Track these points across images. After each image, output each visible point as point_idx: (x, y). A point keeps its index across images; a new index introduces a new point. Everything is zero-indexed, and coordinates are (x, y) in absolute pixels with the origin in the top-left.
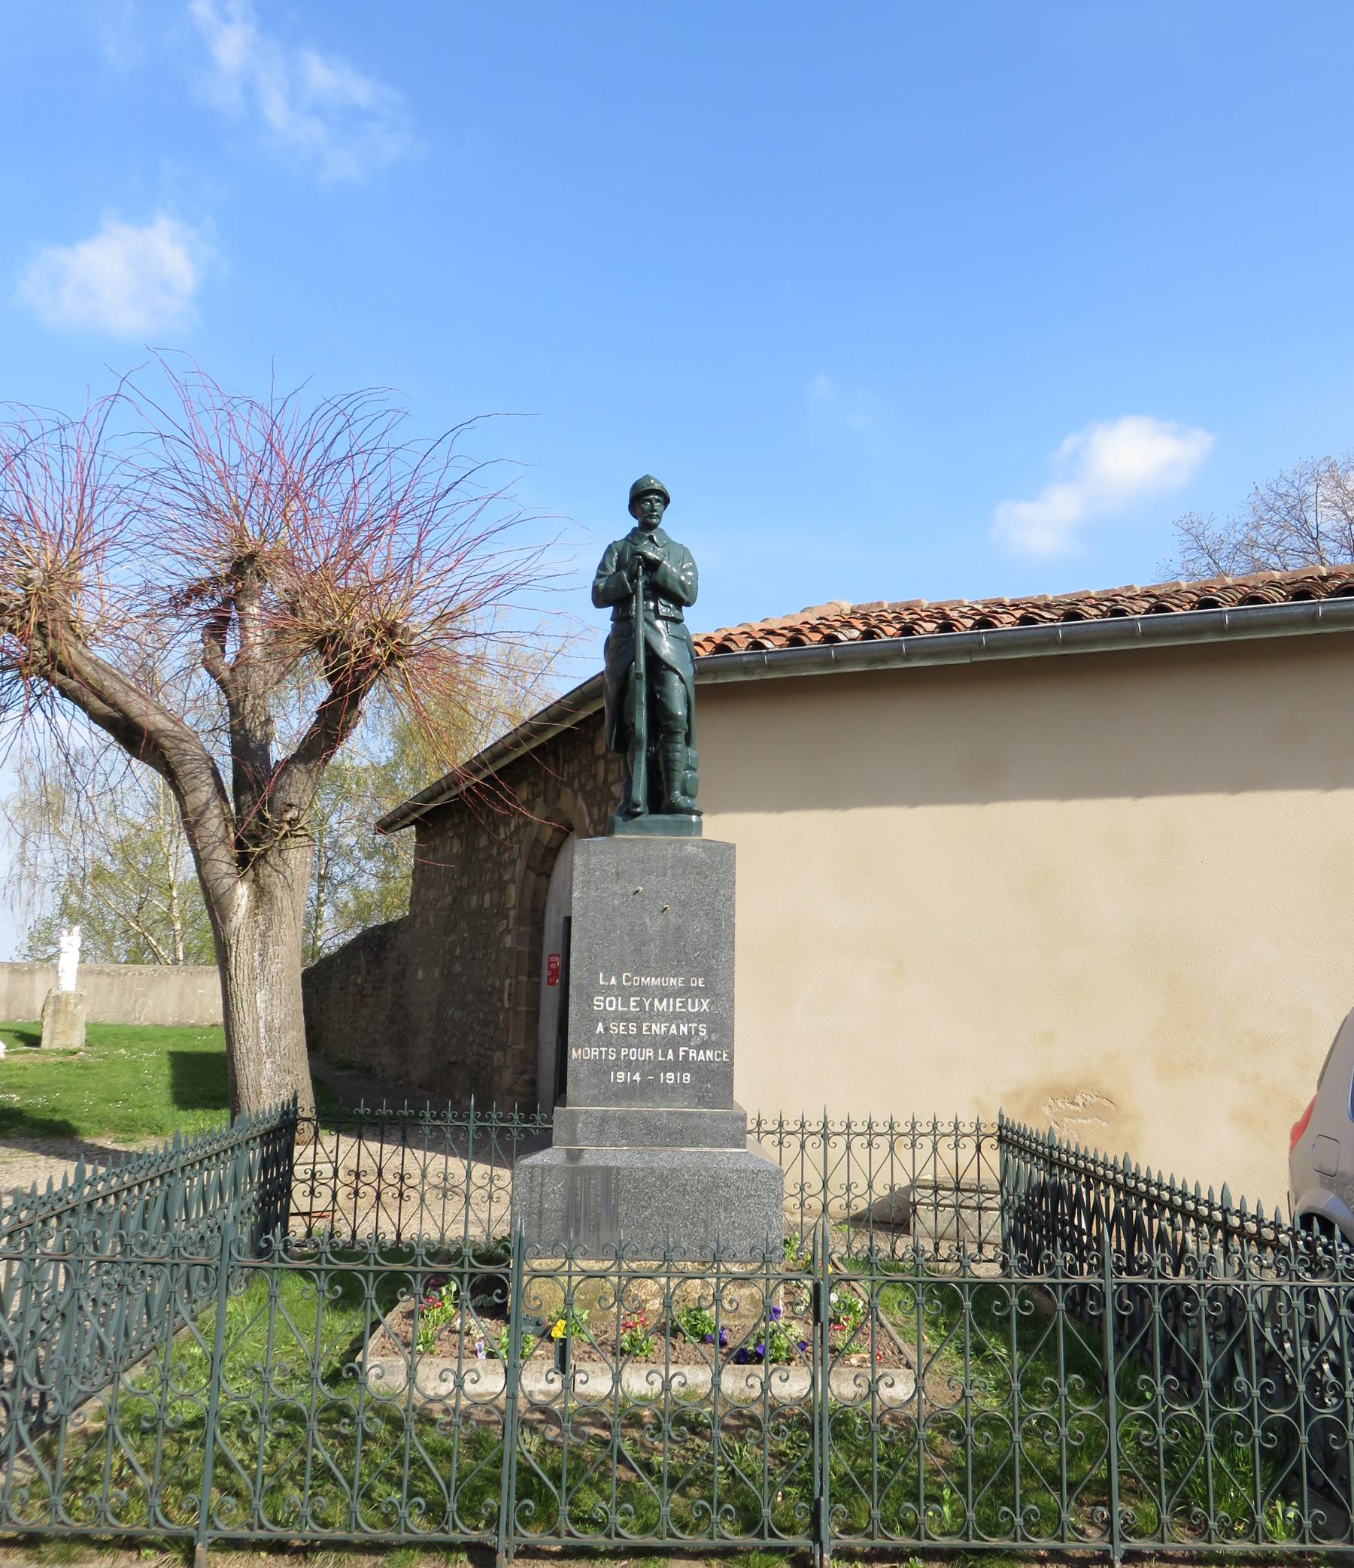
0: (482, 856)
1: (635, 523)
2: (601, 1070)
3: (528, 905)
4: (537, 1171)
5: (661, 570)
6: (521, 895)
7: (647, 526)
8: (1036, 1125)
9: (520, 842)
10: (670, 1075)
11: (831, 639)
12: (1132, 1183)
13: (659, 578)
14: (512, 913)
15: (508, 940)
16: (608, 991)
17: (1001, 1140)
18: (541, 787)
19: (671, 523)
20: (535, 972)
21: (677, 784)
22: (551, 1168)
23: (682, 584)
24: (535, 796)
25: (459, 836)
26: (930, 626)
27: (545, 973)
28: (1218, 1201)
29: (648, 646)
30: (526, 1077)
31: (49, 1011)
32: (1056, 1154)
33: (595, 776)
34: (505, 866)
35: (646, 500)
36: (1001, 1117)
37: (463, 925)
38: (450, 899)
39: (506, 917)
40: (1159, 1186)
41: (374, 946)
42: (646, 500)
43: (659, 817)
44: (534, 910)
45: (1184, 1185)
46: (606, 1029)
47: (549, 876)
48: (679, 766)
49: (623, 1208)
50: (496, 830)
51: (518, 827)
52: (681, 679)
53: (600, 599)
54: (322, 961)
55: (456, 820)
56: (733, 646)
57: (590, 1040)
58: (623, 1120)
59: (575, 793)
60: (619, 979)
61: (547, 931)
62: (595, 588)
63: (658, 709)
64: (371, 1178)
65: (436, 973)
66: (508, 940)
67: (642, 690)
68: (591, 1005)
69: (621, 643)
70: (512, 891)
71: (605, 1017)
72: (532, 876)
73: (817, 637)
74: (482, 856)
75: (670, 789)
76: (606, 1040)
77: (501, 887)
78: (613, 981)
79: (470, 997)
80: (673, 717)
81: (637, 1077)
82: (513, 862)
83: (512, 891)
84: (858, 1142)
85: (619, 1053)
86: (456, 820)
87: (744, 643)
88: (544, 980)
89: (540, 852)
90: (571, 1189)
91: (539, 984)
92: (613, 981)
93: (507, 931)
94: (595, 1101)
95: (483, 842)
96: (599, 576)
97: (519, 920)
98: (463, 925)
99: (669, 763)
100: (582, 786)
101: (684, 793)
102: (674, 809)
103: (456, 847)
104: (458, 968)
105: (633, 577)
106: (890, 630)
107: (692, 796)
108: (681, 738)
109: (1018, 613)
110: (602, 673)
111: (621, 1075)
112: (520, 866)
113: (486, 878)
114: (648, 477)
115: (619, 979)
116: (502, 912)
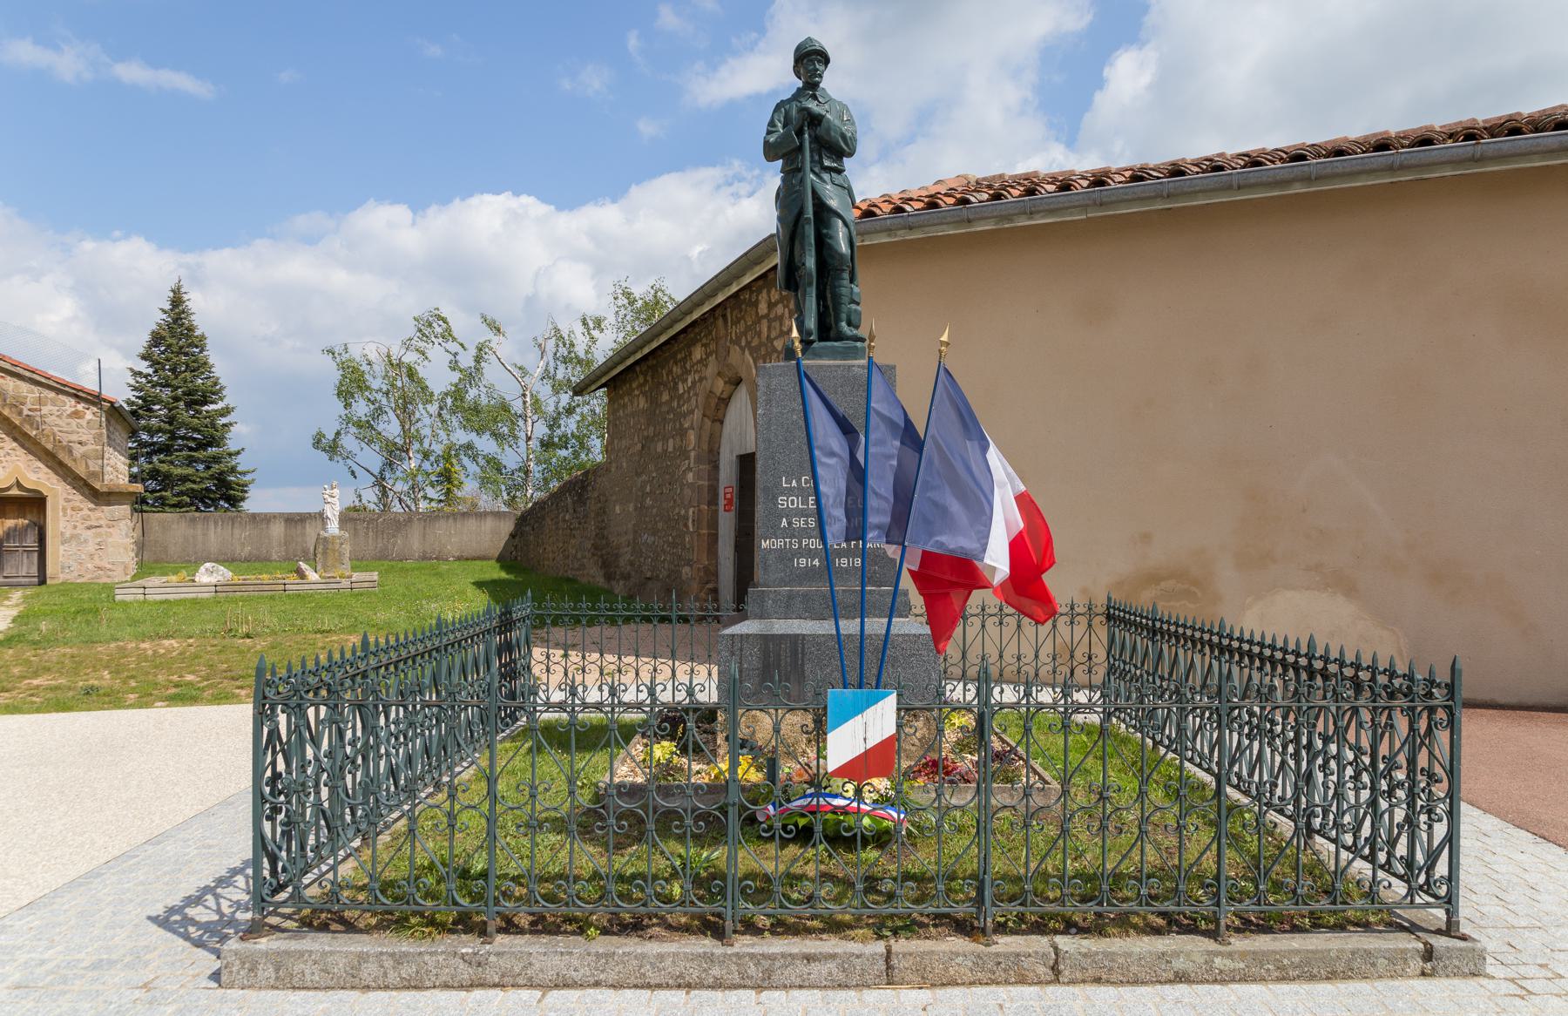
0: (664, 409)
1: (800, 84)
2: (785, 556)
3: (705, 447)
4: (737, 640)
5: (824, 123)
6: (699, 438)
7: (811, 87)
8: (1143, 600)
9: (696, 395)
10: (844, 561)
11: (965, 201)
12: (1225, 642)
13: (820, 131)
14: (693, 454)
15: (690, 477)
16: (790, 492)
17: (1109, 617)
18: (713, 346)
19: (831, 82)
20: (713, 501)
21: (844, 316)
22: (748, 636)
23: (843, 136)
24: (708, 355)
25: (644, 394)
26: (1051, 188)
27: (722, 502)
28: (1304, 651)
29: (814, 192)
30: (710, 586)
31: (320, 550)
32: (1158, 625)
33: (759, 334)
34: (684, 416)
35: (810, 60)
36: (1109, 599)
37: (651, 467)
38: (639, 446)
39: (688, 458)
40: (1251, 642)
41: (579, 489)
42: (810, 60)
43: (829, 344)
44: (711, 451)
45: (1274, 640)
46: (790, 523)
47: (722, 422)
48: (845, 300)
49: (808, 667)
50: (675, 388)
51: (694, 383)
52: (845, 224)
53: (771, 151)
54: (535, 504)
55: (641, 379)
56: (878, 211)
57: (775, 532)
58: (806, 597)
59: (743, 349)
60: (799, 481)
61: (721, 466)
62: (766, 143)
63: (823, 245)
64: (508, 820)
65: (631, 507)
66: (690, 477)
67: (810, 231)
68: (776, 504)
69: (789, 199)
70: (692, 436)
71: (789, 514)
72: (708, 422)
73: (951, 201)
74: (664, 409)
75: (838, 320)
76: (790, 532)
77: (682, 433)
78: (794, 483)
79: (660, 525)
80: (842, 256)
81: (816, 562)
82: (692, 412)
83: (692, 436)
84: (990, 622)
85: (800, 543)
86: (641, 379)
87: (887, 208)
88: (721, 508)
89: (714, 402)
90: (765, 653)
91: (716, 511)
92: (794, 483)
93: (689, 469)
94: (783, 583)
95: (665, 397)
96: (769, 133)
97: (698, 460)
98: (651, 467)
99: (836, 298)
100: (748, 343)
101: (849, 324)
102: (840, 337)
103: (643, 403)
104: (649, 502)
105: (800, 133)
106: (1016, 192)
107: (857, 327)
108: (846, 275)
109: (1128, 174)
110: (772, 236)
111: (803, 561)
112: (697, 415)
113: (669, 427)
114: (809, 39)
115: (799, 481)
116: (684, 454)
